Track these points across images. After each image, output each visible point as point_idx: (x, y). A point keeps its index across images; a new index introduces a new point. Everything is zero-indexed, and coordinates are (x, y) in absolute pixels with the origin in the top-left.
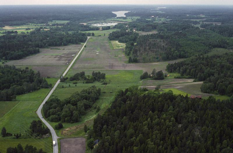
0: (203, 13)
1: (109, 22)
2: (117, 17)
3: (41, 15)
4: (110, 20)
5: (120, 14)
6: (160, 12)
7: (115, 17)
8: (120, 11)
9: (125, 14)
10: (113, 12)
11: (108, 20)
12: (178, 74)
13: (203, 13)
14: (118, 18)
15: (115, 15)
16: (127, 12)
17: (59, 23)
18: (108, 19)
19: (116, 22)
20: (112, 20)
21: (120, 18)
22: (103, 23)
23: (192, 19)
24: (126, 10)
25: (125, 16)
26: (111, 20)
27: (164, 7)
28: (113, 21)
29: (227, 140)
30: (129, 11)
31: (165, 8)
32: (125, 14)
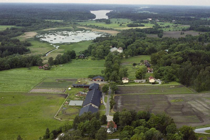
0: (193, 15)
1: (81, 30)
2: (97, 18)
3: (140, 15)
4: (84, 24)
5: (101, 15)
6: (149, 12)
7: (94, 19)
8: (104, 10)
9: (107, 14)
10: (92, 12)
11: (81, 26)
12: (199, 95)
13: (193, 15)
14: (97, 20)
15: (94, 16)
16: (109, 11)
17: (105, 27)
18: (81, 23)
19: (93, 30)
20: (88, 25)
21: (100, 21)
22: (70, 33)
23: (144, 19)
24: (109, 9)
25: (107, 18)
26: (86, 26)
27: (182, 16)
28: (88, 26)
29: (200, 43)
30: (111, 11)
31: (147, 7)
32: (107, 14)
